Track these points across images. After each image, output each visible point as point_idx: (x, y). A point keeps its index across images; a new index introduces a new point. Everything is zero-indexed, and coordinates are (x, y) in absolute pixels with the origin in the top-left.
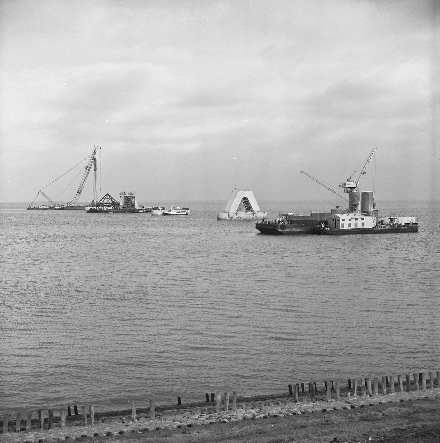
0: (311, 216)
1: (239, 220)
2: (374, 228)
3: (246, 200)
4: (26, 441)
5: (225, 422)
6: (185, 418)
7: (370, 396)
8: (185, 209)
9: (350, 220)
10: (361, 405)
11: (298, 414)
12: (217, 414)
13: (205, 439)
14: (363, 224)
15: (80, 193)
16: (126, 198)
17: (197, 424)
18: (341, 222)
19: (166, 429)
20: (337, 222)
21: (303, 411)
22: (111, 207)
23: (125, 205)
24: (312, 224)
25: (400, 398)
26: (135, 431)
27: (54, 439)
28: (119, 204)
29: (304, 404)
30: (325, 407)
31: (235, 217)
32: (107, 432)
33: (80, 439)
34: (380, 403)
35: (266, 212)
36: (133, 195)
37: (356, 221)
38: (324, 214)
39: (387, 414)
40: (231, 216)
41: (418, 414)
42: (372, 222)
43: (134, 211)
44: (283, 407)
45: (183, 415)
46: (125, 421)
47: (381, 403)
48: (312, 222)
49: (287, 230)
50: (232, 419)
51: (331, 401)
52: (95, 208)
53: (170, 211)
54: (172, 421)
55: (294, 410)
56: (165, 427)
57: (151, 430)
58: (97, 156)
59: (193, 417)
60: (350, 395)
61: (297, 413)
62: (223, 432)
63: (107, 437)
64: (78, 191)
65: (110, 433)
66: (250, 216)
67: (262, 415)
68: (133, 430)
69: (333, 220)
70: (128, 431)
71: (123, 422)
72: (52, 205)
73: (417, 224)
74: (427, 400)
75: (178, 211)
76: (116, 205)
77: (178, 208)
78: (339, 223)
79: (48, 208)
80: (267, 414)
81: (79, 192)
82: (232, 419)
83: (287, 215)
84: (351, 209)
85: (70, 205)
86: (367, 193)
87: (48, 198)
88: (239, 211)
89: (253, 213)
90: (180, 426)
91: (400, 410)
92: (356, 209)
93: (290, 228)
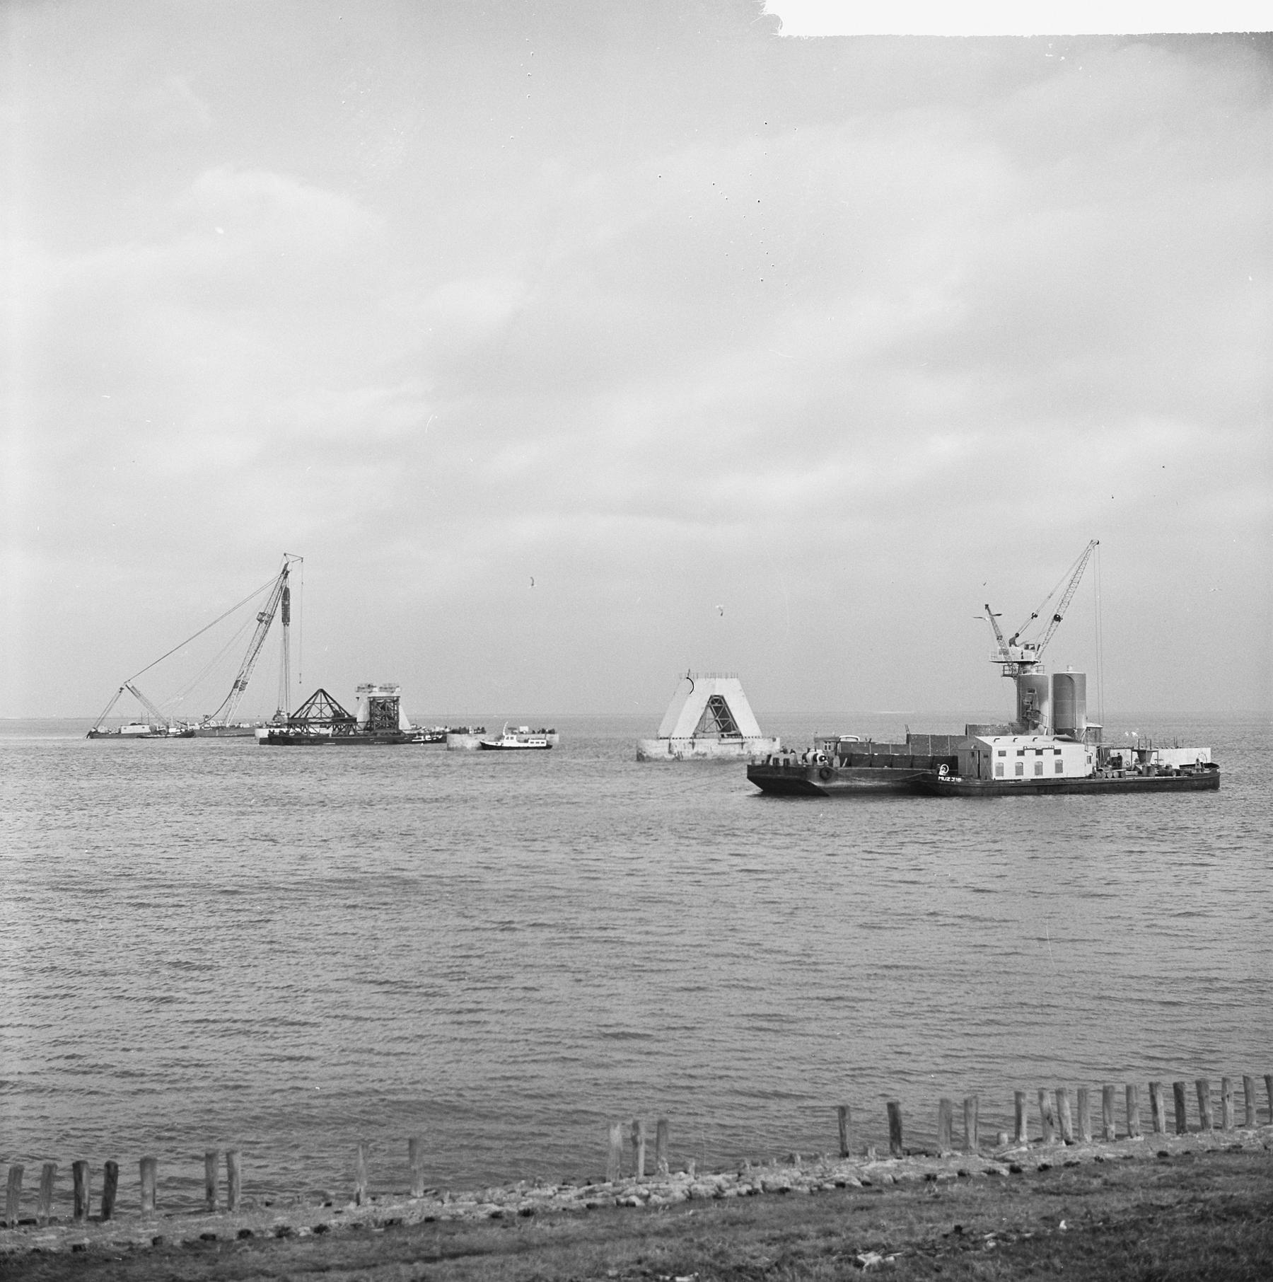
0: (908, 742)
1: (701, 762)
2: (1090, 777)
3: (720, 703)
4: (32, 1247)
5: (633, 1205)
6: (513, 1194)
7: (1068, 1143)
8: (543, 731)
9: (1021, 753)
10: (1039, 1164)
11: (851, 1186)
12: (607, 1184)
13: (570, 1238)
14: (1059, 767)
15: (241, 690)
16: (373, 702)
17: (547, 1210)
18: (995, 759)
19: (455, 1220)
20: (983, 760)
21: (866, 1178)
22: (331, 729)
23: (371, 722)
24: (912, 767)
25: (1158, 1148)
26: (361, 1225)
27: (118, 1244)
28: (355, 720)
29: (870, 1160)
30: (932, 1170)
31: (688, 753)
32: (277, 1227)
33: (196, 1245)
34: (1097, 1159)
35: (778, 739)
36: (394, 695)
37: (1039, 758)
38: (946, 737)
39: (1117, 1181)
40: (675, 751)
41: (1209, 1178)
42: (1085, 760)
43: (397, 738)
44: (806, 1169)
45: (509, 1188)
46: (333, 1200)
47: (1101, 1161)
48: (911, 761)
49: (839, 783)
50: (654, 1197)
51: (952, 1156)
52: (285, 730)
53: (500, 738)
54: (475, 1203)
55: (838, 1176)
56: (452, 1216)
57: (411, 1222)
58: (293, 583)
59: (537, 1191)
60: (1007, 1140)
61: (848, 1182)
62: (626, 1221)
63: (278, 1240)
64: (237, 682)
65: (288, 1228)
66: (730, 748)
67: (744, 1189)
68: (356, 1222)
69: (973, 754)
70: (340, 1225)
71: (328, 1205)
72: (159, 726)
73: (1216, 766)
74: (1237, 1153)
75: (524, 737)
76: (344, 721)
77: (524, 729)
78: (990, 763)
79: (149, 734)
80: (759, 1186)
81: (239, 685)
82: (654, 1197)
83: (837, 741)
84: (1022, 724)
85: (213, 724)
86: (1069, 677)
87: (146, 703)
88: (701, 735)
89: (739, 740)
90: (500, 1212)
91: (1155, 1171)
92: (1037, 724)
93: (847, 778)
